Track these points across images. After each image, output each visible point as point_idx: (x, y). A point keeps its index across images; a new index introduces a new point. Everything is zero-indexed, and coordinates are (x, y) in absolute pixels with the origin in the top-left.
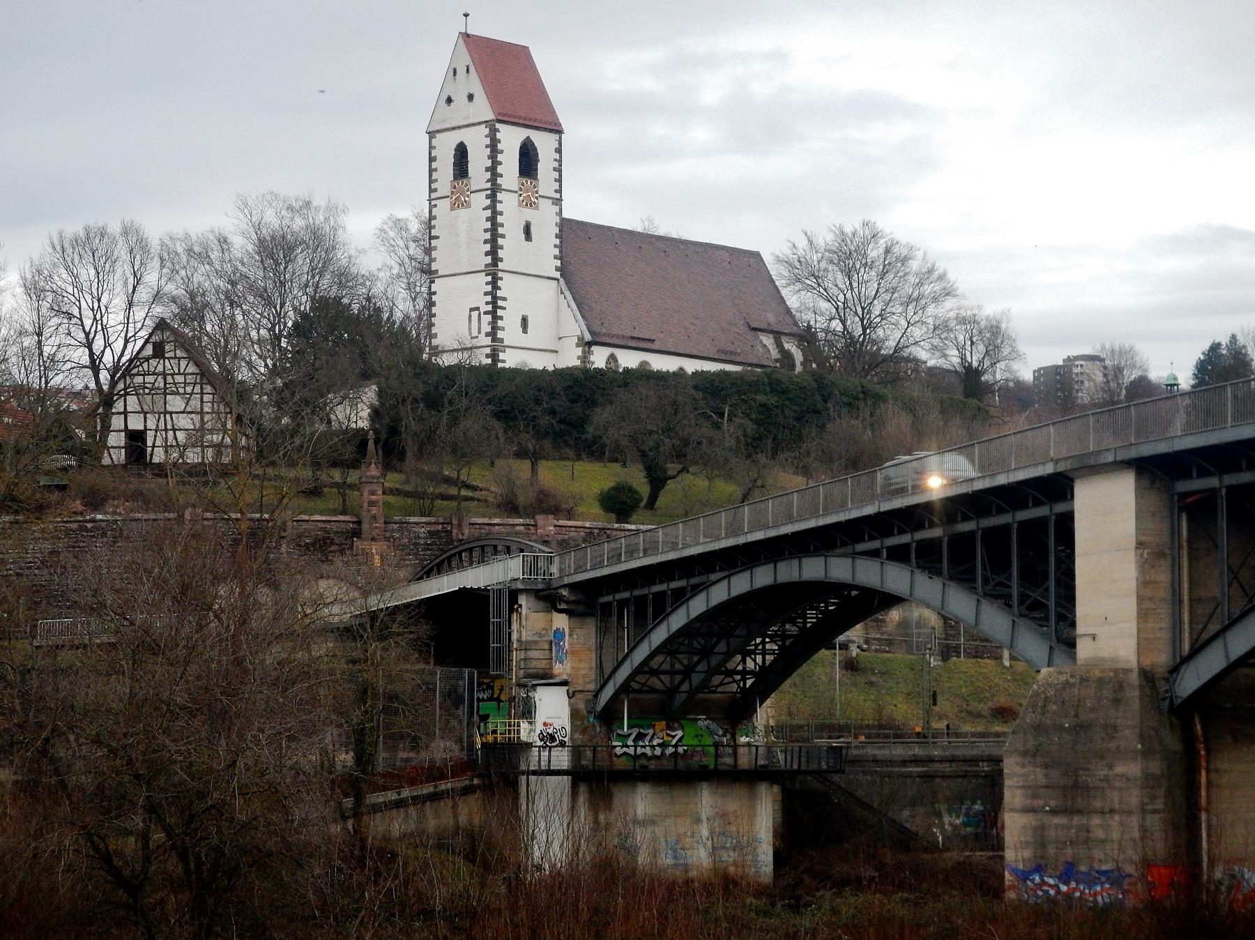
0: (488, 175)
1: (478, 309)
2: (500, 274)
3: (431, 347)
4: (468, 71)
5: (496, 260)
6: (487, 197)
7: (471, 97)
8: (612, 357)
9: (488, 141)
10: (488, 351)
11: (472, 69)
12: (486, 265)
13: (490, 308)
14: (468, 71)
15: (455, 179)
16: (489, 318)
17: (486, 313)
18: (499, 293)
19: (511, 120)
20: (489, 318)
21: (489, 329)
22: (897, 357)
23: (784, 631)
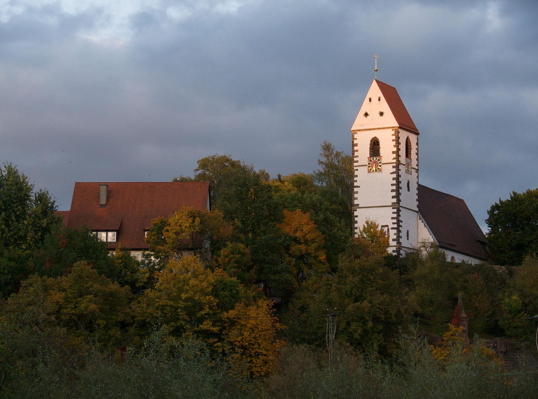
0: (394, 156)
1: (387, 226)
2: (401, 208)
3: (144, 335)
4: (379, 100)
5: (399, 201)
6: (393, 167)
7: (381, 114)
8: (453, 258)
9: (394, 138)
10: (395, 249)
11: (383, 98)
12: (393, 203)
13: (395, 226)
14: (379, 100)
15: (370, 156)
16: (395, 231)
17: (392, 228)
18: (400, 219)
19: (409, 129)
20: (395, 231)
21: (395, 237)
22: (174, 336)
23: (221, 353)
